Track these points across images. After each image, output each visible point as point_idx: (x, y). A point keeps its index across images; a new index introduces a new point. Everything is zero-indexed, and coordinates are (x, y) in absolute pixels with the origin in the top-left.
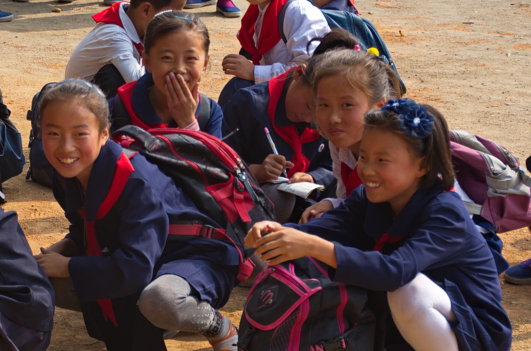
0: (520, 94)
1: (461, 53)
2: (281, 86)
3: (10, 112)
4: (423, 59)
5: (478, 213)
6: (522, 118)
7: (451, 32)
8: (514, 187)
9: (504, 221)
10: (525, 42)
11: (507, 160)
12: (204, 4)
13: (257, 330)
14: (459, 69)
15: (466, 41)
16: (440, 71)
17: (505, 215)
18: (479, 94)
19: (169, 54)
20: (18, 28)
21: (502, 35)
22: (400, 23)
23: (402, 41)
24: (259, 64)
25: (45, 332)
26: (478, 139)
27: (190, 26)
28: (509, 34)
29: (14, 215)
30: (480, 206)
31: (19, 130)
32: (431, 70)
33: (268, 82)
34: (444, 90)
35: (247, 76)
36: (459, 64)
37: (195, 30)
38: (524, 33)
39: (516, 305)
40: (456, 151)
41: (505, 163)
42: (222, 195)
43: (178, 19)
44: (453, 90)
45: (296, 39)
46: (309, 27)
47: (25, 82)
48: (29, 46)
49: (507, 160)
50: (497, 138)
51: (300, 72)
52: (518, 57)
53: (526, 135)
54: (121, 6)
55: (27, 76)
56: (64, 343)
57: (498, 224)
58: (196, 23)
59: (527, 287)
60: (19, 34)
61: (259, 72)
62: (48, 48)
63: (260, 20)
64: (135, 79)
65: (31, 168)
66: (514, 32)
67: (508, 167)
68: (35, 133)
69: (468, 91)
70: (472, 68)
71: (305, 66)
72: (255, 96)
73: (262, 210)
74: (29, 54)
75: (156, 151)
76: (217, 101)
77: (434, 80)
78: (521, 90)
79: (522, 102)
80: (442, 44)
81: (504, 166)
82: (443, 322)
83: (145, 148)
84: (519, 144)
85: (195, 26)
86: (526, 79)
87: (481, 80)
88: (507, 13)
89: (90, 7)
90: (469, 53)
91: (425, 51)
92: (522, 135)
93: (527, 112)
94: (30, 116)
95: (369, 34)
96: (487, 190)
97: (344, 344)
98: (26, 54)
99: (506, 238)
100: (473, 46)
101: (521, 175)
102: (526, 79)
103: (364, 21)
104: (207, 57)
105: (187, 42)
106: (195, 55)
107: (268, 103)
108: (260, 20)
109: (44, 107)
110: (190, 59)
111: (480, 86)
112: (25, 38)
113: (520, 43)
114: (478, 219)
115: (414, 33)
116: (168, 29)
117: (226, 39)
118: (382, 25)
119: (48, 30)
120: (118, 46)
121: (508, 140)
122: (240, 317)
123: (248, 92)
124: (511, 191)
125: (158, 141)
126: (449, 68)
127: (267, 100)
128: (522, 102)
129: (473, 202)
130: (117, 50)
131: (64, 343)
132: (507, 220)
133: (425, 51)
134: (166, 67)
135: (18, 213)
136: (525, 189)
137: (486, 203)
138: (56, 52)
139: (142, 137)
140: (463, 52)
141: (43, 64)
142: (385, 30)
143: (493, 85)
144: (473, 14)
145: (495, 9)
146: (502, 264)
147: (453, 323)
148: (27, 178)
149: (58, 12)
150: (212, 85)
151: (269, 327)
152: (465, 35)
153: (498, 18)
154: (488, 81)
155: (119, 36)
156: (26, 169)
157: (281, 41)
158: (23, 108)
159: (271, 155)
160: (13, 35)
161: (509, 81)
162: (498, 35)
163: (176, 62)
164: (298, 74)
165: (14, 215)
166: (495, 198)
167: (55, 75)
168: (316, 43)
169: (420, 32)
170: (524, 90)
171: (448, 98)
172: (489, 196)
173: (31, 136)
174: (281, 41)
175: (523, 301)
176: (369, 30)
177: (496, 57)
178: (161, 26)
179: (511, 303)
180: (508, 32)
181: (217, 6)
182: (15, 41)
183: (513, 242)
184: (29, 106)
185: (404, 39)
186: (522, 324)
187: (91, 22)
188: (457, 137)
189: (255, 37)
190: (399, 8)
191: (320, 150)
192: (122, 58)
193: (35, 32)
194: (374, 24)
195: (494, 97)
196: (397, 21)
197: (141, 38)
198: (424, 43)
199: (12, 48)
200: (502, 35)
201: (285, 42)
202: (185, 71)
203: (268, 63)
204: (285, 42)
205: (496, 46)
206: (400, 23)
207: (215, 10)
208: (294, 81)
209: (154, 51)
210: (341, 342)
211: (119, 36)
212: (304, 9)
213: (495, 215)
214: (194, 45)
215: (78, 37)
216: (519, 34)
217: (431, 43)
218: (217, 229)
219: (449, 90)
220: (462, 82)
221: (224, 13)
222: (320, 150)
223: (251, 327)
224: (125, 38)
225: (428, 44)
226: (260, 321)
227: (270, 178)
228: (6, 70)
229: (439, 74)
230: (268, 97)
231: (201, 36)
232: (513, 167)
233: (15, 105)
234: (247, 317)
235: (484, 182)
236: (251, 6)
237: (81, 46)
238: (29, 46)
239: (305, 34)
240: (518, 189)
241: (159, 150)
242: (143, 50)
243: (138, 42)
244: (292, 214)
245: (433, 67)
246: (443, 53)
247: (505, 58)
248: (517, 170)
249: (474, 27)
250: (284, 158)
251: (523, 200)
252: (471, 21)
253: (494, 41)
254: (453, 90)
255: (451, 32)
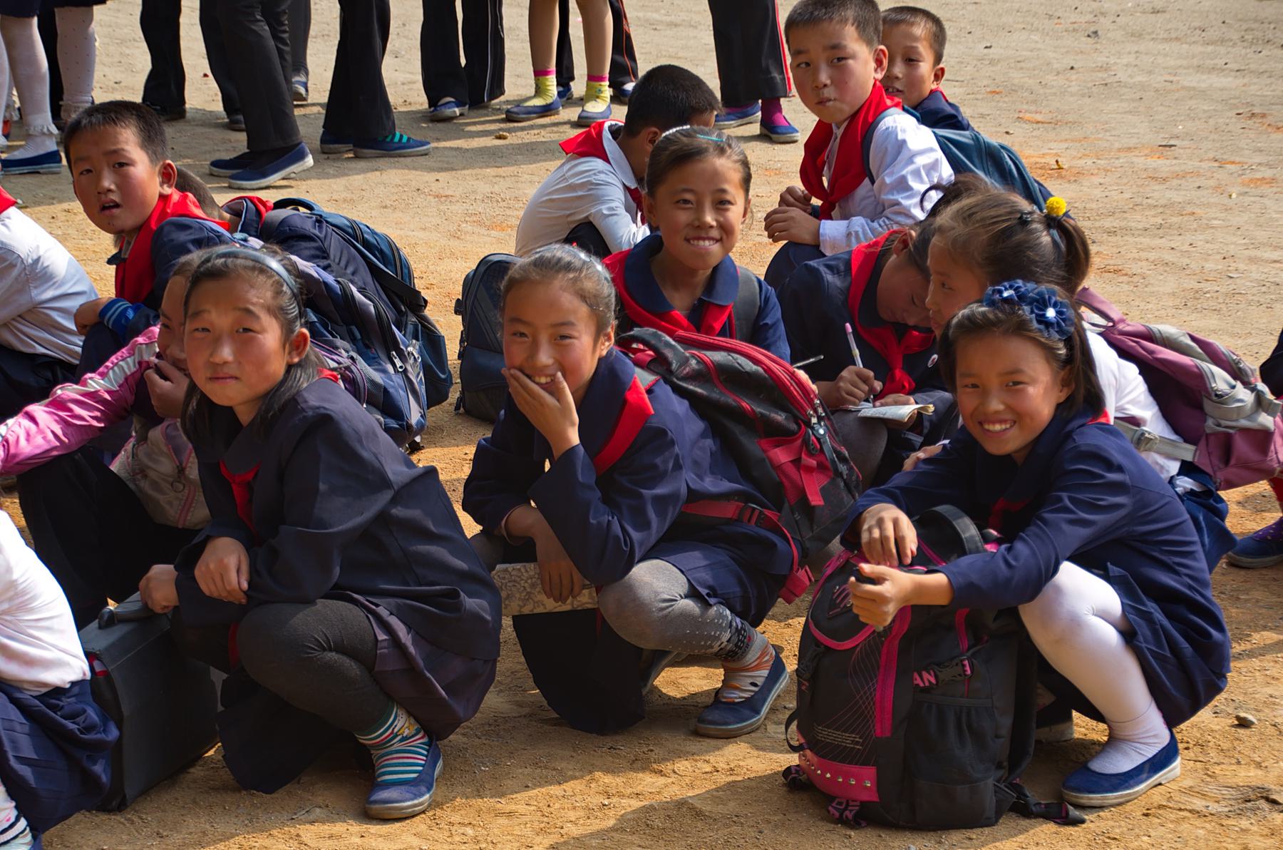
0: (1252, 260)
1: (1156, 195)
2: (873, 259)
3: (426, 302)
4: (1094, 206)
5: (1189, 458)
6: (1256, 298)
7: (1140, 161)
8: (1249, 417)
9: (1231, 472)
10: (1259, 175)
11: (1237, 373)
12: (740, 122)
13: (828, 649)
14: (1153, 220)
15: (1164, 175)
16: (1123, 224)
17: (1233, 462)
18: (1187, 261)
19: (688, 196)
20: (440, 165)
21: (1222, 164)
22: (1057, 147)
23: (1060, 177)
24: (831, 218)
25: (486, 661)
26: (1193, 338)
27: (721, 151)
28: (1233, 163)
29: (431, 472)
30: (1192, 448)
31: (442, 331)
32: (1108, 223)
33: (850, 252)
34: (1129, 256)
35: (807, 238)
36: (1152, 213)
37: (729, 157)
38: (1258, 160)
39: (1247, 601)
40: (1157, 359)
41: (1235, 378)
42: (781, 456)
43: (702, 139)
44: (1144, 255)
45: (888, 180)
46: (911, 161)
47: (452, 254)
48: (457, 194)
49: (1237, 373)
50: (1214, 332)
51: (905, 243)
52: (1247, 199)
53: (1262, 326)
54: (607, 125)
55: (454, 243)
56: (519, 675)
57: (1220, 477)
58: (730, 146)
59: (1264, 572)
60: (442, 176)
61: (828, 232)
62: (489, 198)
63: (834, 145)
64: (625, 248)
65: (462, 392)
66: (1242, 159)
67: (1239, 385)
68: (469, 337)
69: (1169, 257)
70: (1174, 219)
71: (914, 233)
72: (829, 277)
73: (842, 484)
74: (458, 208)
75: (688, 378)
76: (762, 278)
77: (1113, 239)
78: (1253, 253)
79: (1256, 272)
80: (1125, 181)
81: (1233, 382)
82: (1111, 635)
83: (671, 372)
84: (1250, 341)
85: (729, 151)
86: (1261, 235)
87: (1188, 238)
88: (1229, 128)
89: (555, 129)
90: (1169, 194)
91: (1098, 192)
92: (1256, 325)
93: (1264, 289)
94: (460, 308)
95: (1010, 170)
96: (1205, 421)
97: (968, 668)
98: (454, 208)
99: (1230, 496)
100: (1175, 182)
101: (1259, 397)
102: (1261, 235)
103: (1003, 147)
104: (747, 201)
105: (716, 176)
106: (728, 197)
107: (849, 289)
108: (834, 145)
109: (489, 286)
110: (721, 204)
111: (1186, 247)
112: (452, 182)
113: (1251, 176)
114: (1187, 469)
115: (1082, 162)
116: (687, 156)
117: (776, 178)
118: (1028, 152)
119: (487, 167)
120: (600, 192)
121: (1233, 335)
122: (801, 628)
123: (818, 270)
124: (1244, 423)
125: (693, 362)
126: (1138, 220)
127: (846, 284)
128: (1256, 272)
129: (1180, 440)
130: (598, 200)
131: (519, 675)
132: (1234, 470)
133: (1098, 192)
134: (683, 217)
135: (439, 466)
136: (1266, 420)
137: (1203, 442)
138: (502, 204)
139: (669, 354)
140: (1160, 194)
141: (480, 223)
142: (1033, 160)
143: (1208, 246)
144: (1175, 131)
145: (1212, 122)
146: (1223, 539)
147: (1128, 635)
148: (457, 408)
149: (505, 138)
150: (753, 255)
151: (848, 644)
152: (1163, 165)
153: (1216, 137)
154: (1199, 239)
155: (602, 177)
156: (454, 394)
157: (867, 181)
158: (449, 295)
159: (851, 367)
160: (430, 177)
161: (1234, 239)
162: (1216, 164)
163: (699, 209)
164: (901, 246)
165: (431, 472)
166: (1216, 434)
167: (499, 241)
168: (935, 196)
169: (1090, 162)
170: (1258, 253)
171: (1135, 268)
172: (1208, 431)
173: (462, 341)
174: (867, 181)
175: (1257, 594)
176: (1010, 162)
177: (1212, 200)
178: (674, 151)
179: (1238, 599)
180: (1232, 159)
181: (762, 124)
182: (435, 187)
183: (1240, 499)
184: (457, 292)
185: (1064, 173)
186: (1256, 631)
187: (557, 154)
188: (1158, 335)
189: (824, 179)
190: (1055, 123)
191: (930, 364)
192: (605, 212)
193: (466, 172)
194: (1015, 149)
195: (1208, 266)
196: (1053, 145)
197: (639, 180)
198: (1096, 180)
199: (431, 198)
200: (1222, 164)
201: (873, 182)
202: (714, 223)
203: (845, 217)
204: (873, 182)
205: (1212, 183)
206: (1057, 147)
207: (758, 132)
208: (894, 256)
209: (662, 191)
210: (964, 666)
211: (602, 177)
212: (904, 131)
213: (1216, 461)
214: (726, 181)
215: (536, 179)
216: (1250, 161)
217: (1107, 179)
218: (767, 512)
219: (1137, 256)
220: (1158, 242)
221: (774, 136)
222: (930, 364)
223: (818, 643)
224: (611, 179)
225: (1102, 181)
226: (833, 634)
227: (845, 401)
228: (421, 234)
229: (1121, 229)
230: (849, 279)
231: (738, 166)
232: (1246, 384)
233: (436, 291)
234: (813, 627)
235: (1200, 407)
236: (819, 124)
237: (541, 193)
238: (457, 194)
239: (904, 172)
240: (1254, 420)
241: (695, 377)
242: (639, 201)
243: (633, 186)
244: (882, 460)
245: (1111, 219)
246: (1127, 196)
247: (1226, 201)
248: (1253, 389)
249: (1176, 151)
250: (871, 374)
251: (1263, 438)
252: (1172, 142)
253: (1209, 174)
254: (1144, 255)
255: (1140, 161)
